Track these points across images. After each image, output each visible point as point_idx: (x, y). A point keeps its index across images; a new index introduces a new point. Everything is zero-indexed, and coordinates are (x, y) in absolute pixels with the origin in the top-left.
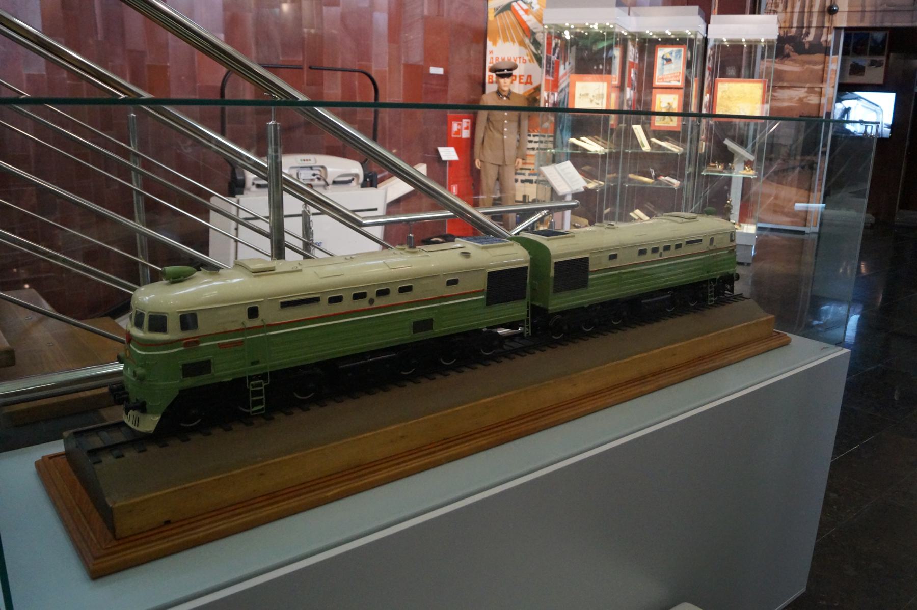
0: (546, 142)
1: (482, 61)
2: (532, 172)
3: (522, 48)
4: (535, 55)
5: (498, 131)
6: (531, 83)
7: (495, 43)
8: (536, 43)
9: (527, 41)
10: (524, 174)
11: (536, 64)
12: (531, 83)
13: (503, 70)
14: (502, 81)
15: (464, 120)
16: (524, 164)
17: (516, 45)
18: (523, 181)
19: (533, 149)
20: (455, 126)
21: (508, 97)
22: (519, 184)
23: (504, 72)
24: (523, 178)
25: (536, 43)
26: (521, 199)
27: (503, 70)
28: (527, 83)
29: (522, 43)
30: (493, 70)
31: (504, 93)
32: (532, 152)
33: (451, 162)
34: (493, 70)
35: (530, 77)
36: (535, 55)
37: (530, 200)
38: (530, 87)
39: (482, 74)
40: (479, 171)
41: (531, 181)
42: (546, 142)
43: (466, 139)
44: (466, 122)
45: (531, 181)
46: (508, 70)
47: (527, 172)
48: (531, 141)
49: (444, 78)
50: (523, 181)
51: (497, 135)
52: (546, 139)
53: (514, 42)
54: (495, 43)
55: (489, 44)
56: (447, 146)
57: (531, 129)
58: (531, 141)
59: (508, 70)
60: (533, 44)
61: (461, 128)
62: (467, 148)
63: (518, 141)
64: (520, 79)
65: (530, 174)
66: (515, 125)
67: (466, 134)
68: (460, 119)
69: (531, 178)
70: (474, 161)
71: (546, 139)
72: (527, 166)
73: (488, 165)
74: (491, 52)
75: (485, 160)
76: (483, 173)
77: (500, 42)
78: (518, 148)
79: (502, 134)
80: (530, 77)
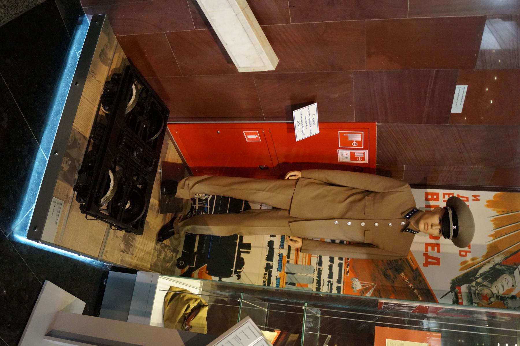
0: (330, 284)
1: (461, 183)
2: (285, 259)
3: (485, 251)
4: (476, 271)
5: (348, 210)
6: (426, 264)
7: (491, 204)
8: (494, 275)
9: (498, 259)
10: (282, 246)
11: (458, 273)
12: (426, 264)
13: (456, 223)
14: (436, 220)
15: (366, 152)
16: (297, 250)
17: (490, 241)
18: (271, 244)
19: (320, 263)
20: (355, 137)
21: (405, 229)
22: (267, 238)
23: (453, 221)
24: (276, 245)
25: (494, 275)
26: (245, 241)
27: (456, 223)
28: (426, 255)
29: (493, 250)
30: (454, 204)
31: (488, 297)
32: (314, 261)
33: (291, 128)
34: (454, 204)
35: (437, 262)
36: (476, 271)
37: (242, 255)
38: (420, 261)
39: (440, 183)
40: (282, 177)
41: (270, 257)
42: (330, 284)
43: (335, 156)
44: (363, 155)
45: (270, 257)
46: (456, 231)
47: (285, 252)
48: (332, 260)
49: (443, 115)
50: (271, 244)
51: (342, 207)
52: (335, 285)
53: (495, 236)
54: (491, 204)
55: (490, 195)
56: (320, 122)
57: (352, 264)
58: (332, 260)
59: (456, 231)
60: (493, 268)
61: (353, 146)
62: (317, 158)
63: (333, 241)
64: (433, 245)
65: (281, 256)
66: (358, 237)
67: (344, 156)
68: (367, 144)
69: (276, 258)
70: (299, 170)
71: (335, 285)
72: (293, 252)
73: (290, 192)
74: (476, 198)
75: (300, 191)
76: (279, 183)
77: (493, 213)
78: (322, 242)
79: (341, 218)
80: (437, 262)
